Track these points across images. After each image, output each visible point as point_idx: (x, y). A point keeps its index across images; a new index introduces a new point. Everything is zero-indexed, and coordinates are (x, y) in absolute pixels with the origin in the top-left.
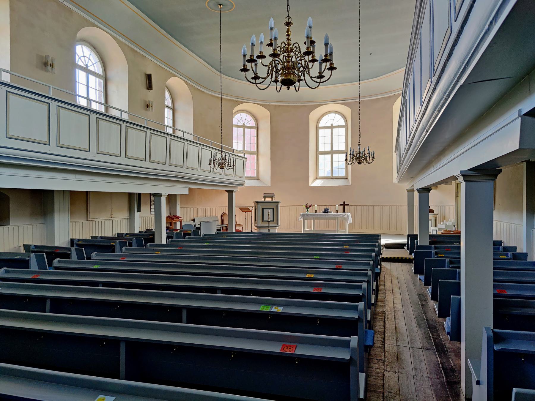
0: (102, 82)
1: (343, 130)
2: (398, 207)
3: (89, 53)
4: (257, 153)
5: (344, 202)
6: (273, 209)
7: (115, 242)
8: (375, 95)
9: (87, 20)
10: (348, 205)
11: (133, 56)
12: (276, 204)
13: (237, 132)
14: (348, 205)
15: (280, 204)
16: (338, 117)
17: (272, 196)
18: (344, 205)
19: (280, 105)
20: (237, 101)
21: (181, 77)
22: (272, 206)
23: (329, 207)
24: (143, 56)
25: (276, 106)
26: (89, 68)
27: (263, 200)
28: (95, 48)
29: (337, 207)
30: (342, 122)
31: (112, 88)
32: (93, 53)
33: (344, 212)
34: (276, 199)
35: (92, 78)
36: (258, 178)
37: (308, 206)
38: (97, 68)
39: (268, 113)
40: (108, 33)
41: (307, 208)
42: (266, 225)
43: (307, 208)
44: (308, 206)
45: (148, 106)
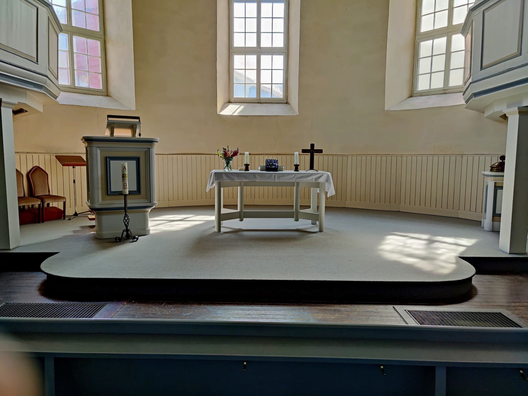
2: (394, 158)
4: (103, 35)
5: (312, 146)
6: (138, 160)
14: (320, 151)
15: (156, 149)
17: (132, 122)
18: (312, 151)
23: (278, 158)
27: (107, 134)
29: (297, 158)
33: (312, 168)
34: (144, 132)
36: (106, 93)
37: (230, 154)
41: (228, 158)
43: (228, 158)
44: (230, 154)
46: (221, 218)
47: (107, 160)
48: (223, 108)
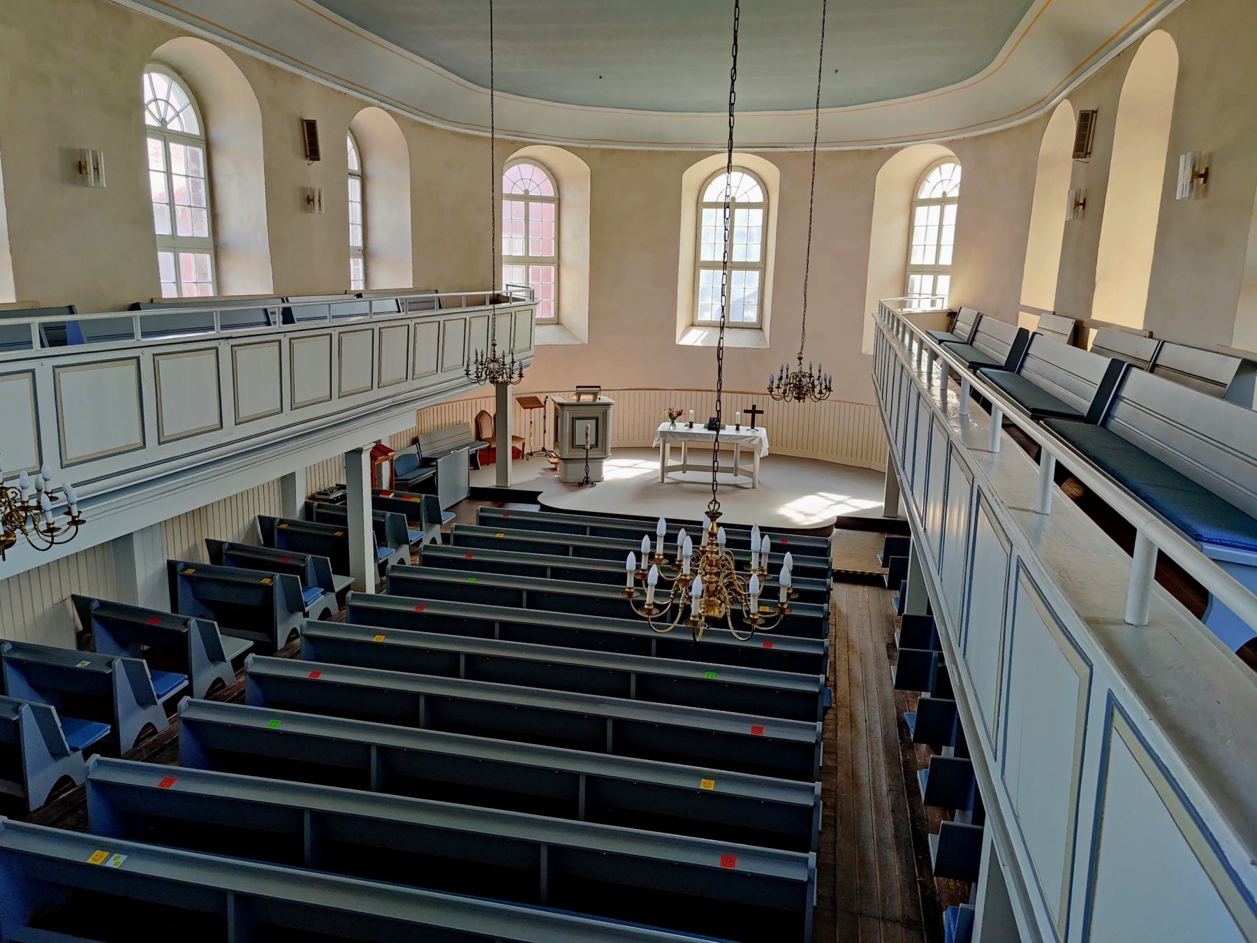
0: (200, 152)
1: (758, 215)
3: (166, 86)
4: (558, 262)
5: (754, 407)
6: (597, 419)
7: (272, 577)
8: (836, 143)
9: (162, 24)
10: (762, 412)
11: (266, 80)
12: (604, 408)
13: (511, 212)
14: (762, 412)
15: (611, 411)
16: (749, 181)
17: (595, 390)
18: (754, 411)
19: (613, 151)
20: (513, 142)
21: (383, 105)
22: (596, 412)
24: (294, 76)
25: (604, 151)
26: (170, 127)
28: (179, 73)
30: (758, 196)
31: (223, 168)
32: (175, 86)
34: (603, 398)
35: (177, 149)
36: (557, 322)
38: (188, 122)
39: (585, 168)
40: (359, 406)
42: (582, 454)
44: (675, 414)
45: (309, 200)
46: (665, 470)
47: (573, 420)
48: (685, 333)
